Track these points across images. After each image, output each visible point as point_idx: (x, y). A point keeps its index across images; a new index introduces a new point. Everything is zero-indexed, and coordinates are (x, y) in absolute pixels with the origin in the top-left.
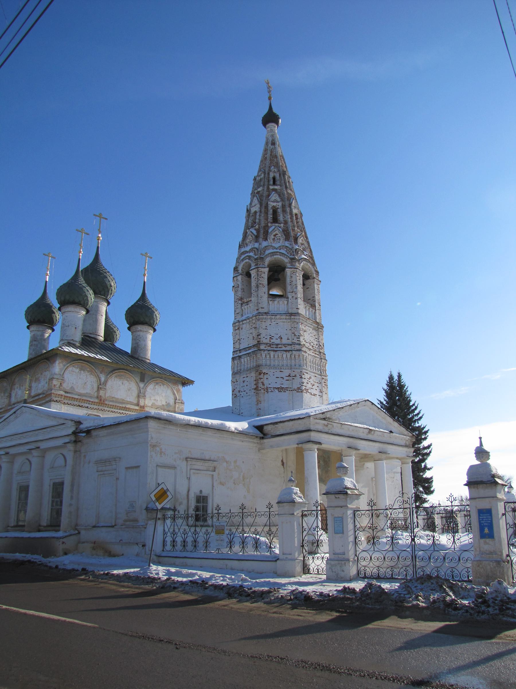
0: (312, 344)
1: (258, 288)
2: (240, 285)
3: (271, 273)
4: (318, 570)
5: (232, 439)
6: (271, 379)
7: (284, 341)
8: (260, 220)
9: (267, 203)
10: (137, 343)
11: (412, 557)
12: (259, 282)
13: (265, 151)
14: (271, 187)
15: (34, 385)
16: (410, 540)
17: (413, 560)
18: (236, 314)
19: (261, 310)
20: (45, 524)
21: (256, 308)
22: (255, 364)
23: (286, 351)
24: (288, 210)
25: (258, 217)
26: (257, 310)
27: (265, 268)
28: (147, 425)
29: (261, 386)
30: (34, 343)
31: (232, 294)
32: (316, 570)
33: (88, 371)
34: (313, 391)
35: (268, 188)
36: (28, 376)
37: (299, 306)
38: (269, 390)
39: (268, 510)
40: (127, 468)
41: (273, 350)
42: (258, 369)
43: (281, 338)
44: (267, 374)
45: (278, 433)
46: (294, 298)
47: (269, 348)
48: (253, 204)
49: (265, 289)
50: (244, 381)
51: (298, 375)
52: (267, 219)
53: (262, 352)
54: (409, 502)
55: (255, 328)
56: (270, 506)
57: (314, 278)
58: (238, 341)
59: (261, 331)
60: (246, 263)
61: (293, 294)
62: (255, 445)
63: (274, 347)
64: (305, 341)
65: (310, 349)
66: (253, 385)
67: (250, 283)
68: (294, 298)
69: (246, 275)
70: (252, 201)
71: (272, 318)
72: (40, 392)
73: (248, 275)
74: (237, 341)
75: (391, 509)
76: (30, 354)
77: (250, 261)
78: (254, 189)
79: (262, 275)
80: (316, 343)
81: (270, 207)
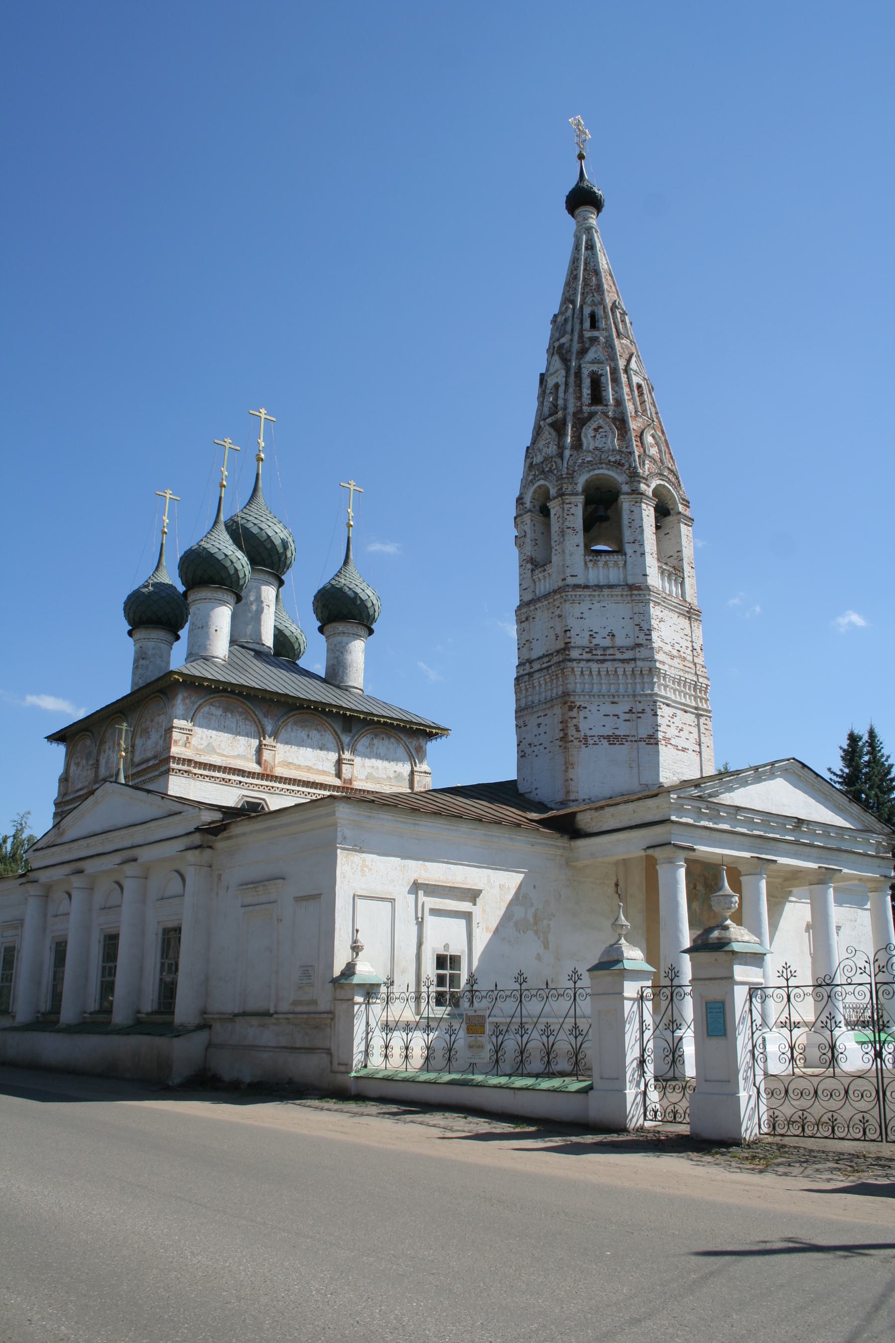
0: (677, 647)
1: (563, 536)
2: (528, 532)
3: (591, 508)
4: (675, 1113)
5: (511, 839)
6: (594, 720)
7: (620, 641)
8: (565, 400)
9: (580, 366)
10: (337, 658)
11: (877, 1092)
12: (567, 524)
13: (574, 263)
14: (587, 334)
15: (139, 742)
16: (872, 1053)
17: (879, 1099)
18: (523, 590)
19: (570, 581)
20: (149, 1010)
21: (562, 577)
22: (561, 688)
23: (623, 661)
24: (624, 378)
25: (561, 394)
26: (564, 580)
27: (577, 494)
28: (333, 813)
29: (574, 732)
30: (142, 662)
31: (515, 551)
32: (672, 1115)
33: (241, 714)
34: (681, 743)
35: (581, 336)
36: (125, 724)
37: (648, 571)
38: (590, 741)
39: (517, 986)
40: (298, 899)
41: (598, 661)
42: (566, 700)
43: (613, 635)
44: (585, 708)
45: (605, 828)
46: (638, 554)
47: (589, 656)
48: (552, 370)
49: (580, 538)
50: (539, 725)
51: (648, 710)
52: (580, 398)
53: (575, 664)
54: (867, 970)
55: (560, 616)
56: (575, 976)
57: (680, 513)
58: (527, 645)
59: (571, 622)
60: (540, 487)
61: (636, 546)
62: (559, 852)
63: (599, 654)
64: (662, 641)
65: (673, 657)
66: (557, 731)
67: (548, 526)
68: (638, 554)
69: (541, 512)
70: (549, 363)
71: (594, 596)
72: (149, 754)
73: (545, 512)
74: (524, 644)
75: (828, 985)
76: (134, 683)
77: (547, 483)
78: (553, 339)
79: (572, 511)
80: (685, 644)
81: (585, 373)
